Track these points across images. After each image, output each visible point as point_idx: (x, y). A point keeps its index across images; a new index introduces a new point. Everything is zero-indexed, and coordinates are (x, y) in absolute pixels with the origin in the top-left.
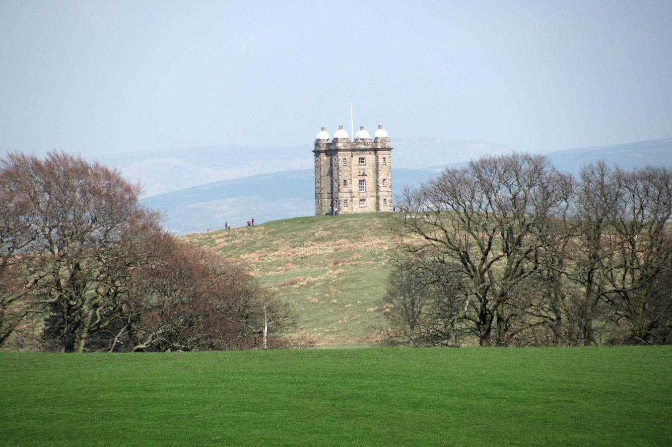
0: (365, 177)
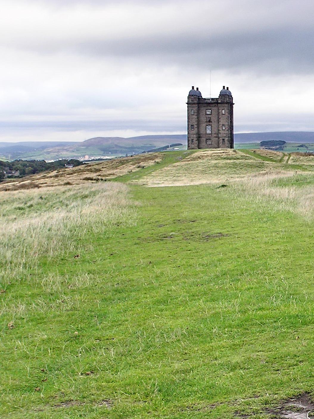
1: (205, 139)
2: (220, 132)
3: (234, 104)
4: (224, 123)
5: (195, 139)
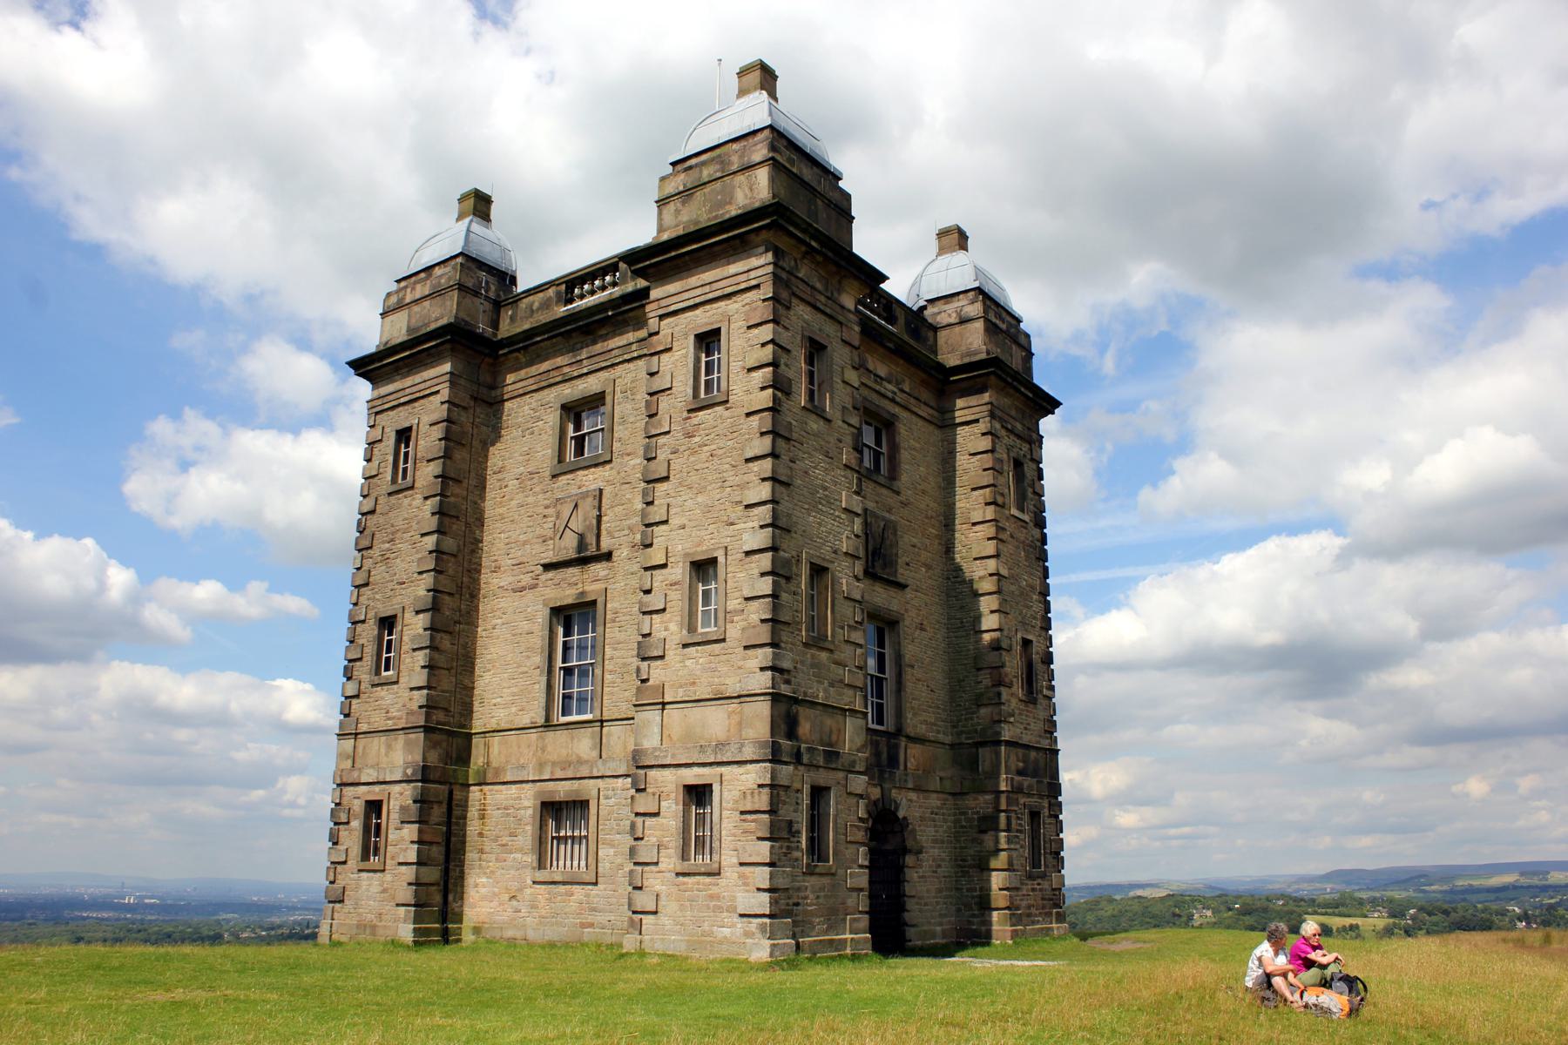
3: (365, 367)
5: (400, 798)
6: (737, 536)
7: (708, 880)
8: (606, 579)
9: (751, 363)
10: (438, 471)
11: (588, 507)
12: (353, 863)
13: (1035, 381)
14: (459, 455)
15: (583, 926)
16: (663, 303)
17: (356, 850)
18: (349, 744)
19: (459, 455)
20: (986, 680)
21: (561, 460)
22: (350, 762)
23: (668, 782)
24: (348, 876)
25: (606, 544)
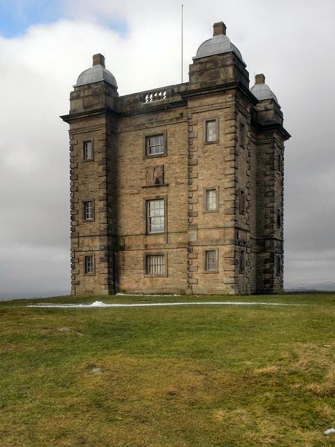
0: (165, 189)
1: (140, 255)
2: (195, 221)
3: (65, 118)
4: (213, 183)
5: (99, 255)
6: (223, 183)
7: (214, 275)
8: (167, 192)
9: (227, 132)
10: (104, 156)
11: (159, 170)
12: (81, 274)
13: (284, 127)
14: (109, 151)
15: (163, 289)
16: (194, 109)
17: (82, 270)
18: (76, 240)
19: (109, 151)
20: (268, 221)
21: (146, 155)
22: (77, 245)
23: (200, 249)
24: (80, 278)
25: (166, 181)
